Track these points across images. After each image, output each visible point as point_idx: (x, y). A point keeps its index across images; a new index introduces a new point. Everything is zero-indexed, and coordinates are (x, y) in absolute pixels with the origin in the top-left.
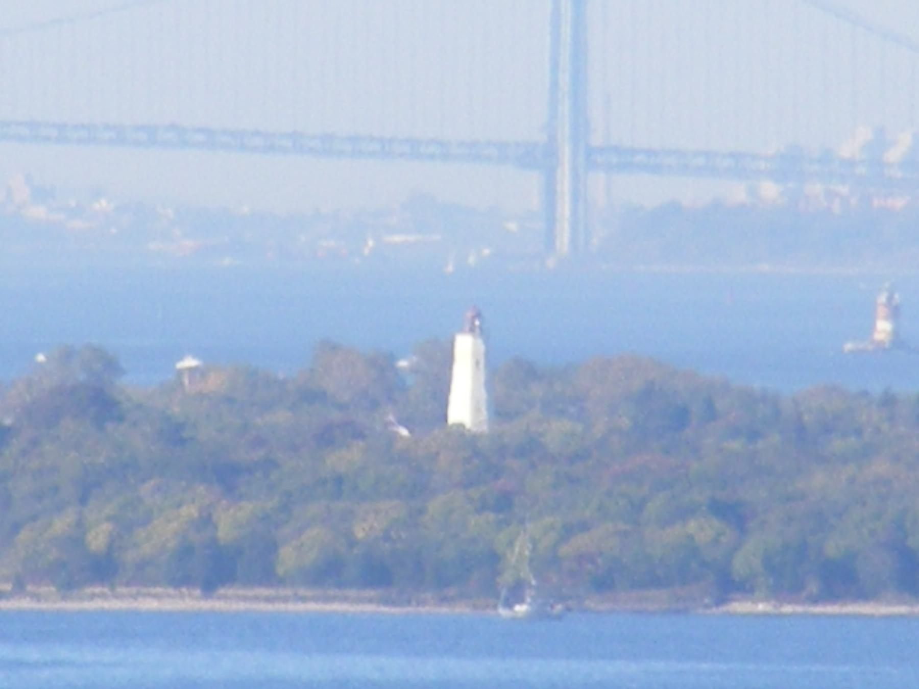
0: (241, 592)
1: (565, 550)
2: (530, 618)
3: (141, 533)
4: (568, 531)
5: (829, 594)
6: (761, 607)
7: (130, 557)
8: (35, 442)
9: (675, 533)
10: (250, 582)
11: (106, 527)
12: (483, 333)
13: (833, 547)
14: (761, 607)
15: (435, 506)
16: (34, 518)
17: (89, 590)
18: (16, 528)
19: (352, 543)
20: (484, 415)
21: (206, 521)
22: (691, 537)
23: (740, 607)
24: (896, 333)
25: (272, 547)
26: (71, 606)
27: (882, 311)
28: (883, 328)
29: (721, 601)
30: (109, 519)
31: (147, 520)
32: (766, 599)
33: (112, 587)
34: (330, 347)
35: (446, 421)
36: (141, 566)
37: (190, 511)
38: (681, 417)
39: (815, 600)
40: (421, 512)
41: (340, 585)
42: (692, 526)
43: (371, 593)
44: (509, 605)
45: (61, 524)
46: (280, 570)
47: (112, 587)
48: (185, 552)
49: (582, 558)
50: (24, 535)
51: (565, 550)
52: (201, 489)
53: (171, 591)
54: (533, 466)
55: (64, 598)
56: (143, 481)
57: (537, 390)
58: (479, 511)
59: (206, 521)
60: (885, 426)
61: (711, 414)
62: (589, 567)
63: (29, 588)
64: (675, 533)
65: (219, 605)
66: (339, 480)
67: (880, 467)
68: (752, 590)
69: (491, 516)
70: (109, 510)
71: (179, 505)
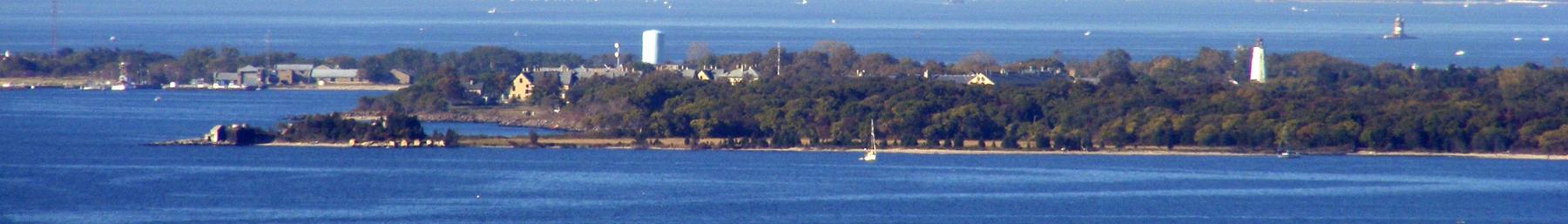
0: (1184, 148)
1: (1298, 132)
2: (1289, 157)
3: (1145, 126)
4: (1300, 125)
5: (1396, 148)
6: (1371, 153)
7: (1141, 135)
8: (1105, 92)
9: (1338, 127)
10: (1185, 145)
11: (1133, 124)
12: (1263, 46)
13: (1396, 132)
14: (1371, 153)
15: (1252, 116)
16: (1108, 121)
17: (1127, 147)
18: (1100, 125)
19: (1221, 130)
20: (1264, 77)
21: (1169, 122)
22: (1345, 127)
23: (1363, 152)
24: (1402, 32)
25: (1193, 132)
26: (1121, 153)
27: (1397, 24)
28: (1398, 30)
29: (1356, 151)
30: (1135, 121)
31: (1148, 120)
32: (1372, 150)
33: (1136, 146)
34: (1205, 50)
35: (1250, 76)
36: (1145, 138)
37: (1163, 119)
38: (1335, 77)
39: (1390, 150)
40: (1247, 118)
41: (1218, 145)
42: (1345, 124)
43: (1227, 148)
44: (1280, 153)
45: (1117, 123)
46: (1196, 140)
47: (1136, 146)
48: (1162, 132)
49: (1306, 135)
50: (1104, 127)
51: (1298, 132)
52: (1167, 110)
53: (1156, 147)
54: (1286, 101)
55: (1119, 151)
56: (1146, 107)
57: (1282, 65)
58: (1269, 117)
59: (1169, 122)
60: (1410, 80)
61: (1346, 76)
62: (1308, 138)
63: (1106, 147)
64: (1338, 127)
65: (1172, 153)
66: (1216, 106)
67: (1412, 103)
68: (1367, 147)
69: (1272, 120)
70: (1135, 117)
71: (1159, 116)
